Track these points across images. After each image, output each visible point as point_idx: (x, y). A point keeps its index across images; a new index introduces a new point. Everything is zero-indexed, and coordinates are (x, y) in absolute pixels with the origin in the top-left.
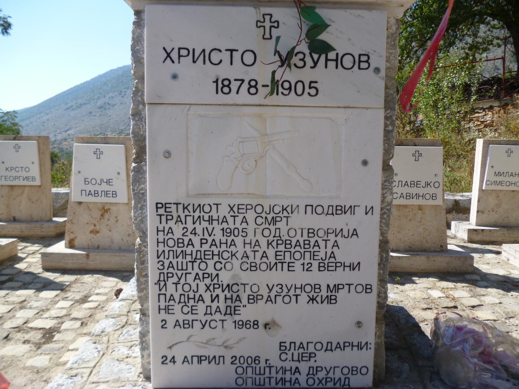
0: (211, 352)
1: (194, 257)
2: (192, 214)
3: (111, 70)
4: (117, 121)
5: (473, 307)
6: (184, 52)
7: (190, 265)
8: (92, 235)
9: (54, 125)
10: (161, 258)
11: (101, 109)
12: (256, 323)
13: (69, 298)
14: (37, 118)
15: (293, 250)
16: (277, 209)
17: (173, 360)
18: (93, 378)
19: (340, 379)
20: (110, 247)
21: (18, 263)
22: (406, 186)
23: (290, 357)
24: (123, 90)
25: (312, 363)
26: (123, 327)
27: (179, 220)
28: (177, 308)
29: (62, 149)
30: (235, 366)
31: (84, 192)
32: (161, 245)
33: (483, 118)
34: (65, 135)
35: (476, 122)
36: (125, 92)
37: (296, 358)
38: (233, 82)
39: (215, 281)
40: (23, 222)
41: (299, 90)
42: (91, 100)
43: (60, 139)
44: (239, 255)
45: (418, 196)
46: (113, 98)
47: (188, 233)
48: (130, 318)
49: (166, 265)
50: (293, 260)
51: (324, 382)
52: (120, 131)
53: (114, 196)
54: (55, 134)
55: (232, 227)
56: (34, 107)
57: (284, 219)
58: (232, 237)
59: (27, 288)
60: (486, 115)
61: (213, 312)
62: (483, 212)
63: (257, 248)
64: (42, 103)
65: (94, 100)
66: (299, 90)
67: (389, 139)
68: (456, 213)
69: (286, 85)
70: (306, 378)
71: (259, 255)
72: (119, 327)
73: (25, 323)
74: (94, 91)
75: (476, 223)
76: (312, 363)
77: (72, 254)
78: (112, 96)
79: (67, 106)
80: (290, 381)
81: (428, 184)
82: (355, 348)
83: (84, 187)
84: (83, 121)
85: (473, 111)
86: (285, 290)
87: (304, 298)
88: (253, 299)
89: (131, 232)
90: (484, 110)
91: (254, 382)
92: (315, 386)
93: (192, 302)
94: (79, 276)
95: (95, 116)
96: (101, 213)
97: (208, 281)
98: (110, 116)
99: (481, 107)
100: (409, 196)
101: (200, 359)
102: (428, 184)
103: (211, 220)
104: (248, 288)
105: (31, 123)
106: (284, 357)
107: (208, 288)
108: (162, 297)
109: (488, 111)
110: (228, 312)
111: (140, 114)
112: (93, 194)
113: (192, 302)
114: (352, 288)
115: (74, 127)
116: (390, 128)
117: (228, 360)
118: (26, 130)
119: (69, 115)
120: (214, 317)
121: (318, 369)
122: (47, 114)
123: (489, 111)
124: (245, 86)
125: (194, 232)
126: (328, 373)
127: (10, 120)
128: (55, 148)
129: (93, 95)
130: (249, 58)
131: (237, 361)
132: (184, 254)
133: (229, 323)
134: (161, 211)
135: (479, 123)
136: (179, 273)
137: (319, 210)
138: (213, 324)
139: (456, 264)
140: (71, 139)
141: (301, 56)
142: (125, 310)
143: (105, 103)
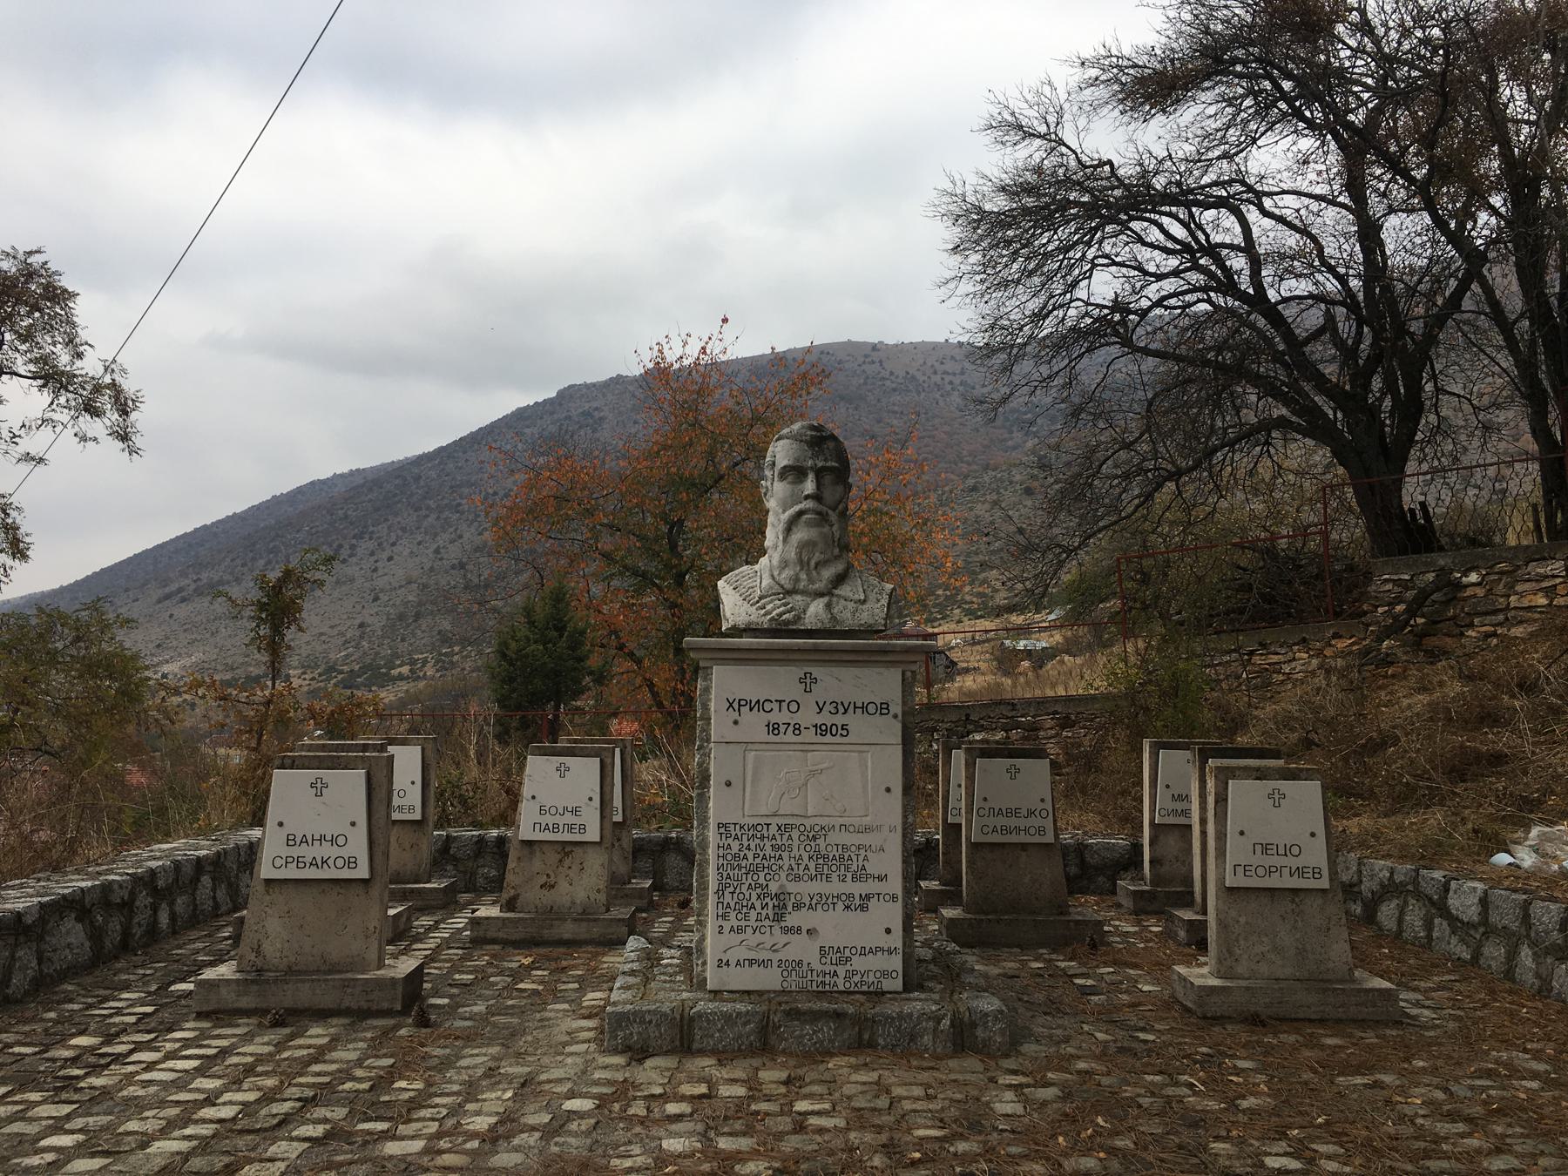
3: (312, 483)
12: (799, 929)
17: (728, 964)
25: (848, 967)
27: (736, 837)
28: (733, 915)
31: (537, 826)
44: (785, 868)
45: (1018, 830)
71: (802, 868)
74: (254, 544)
76: (848, 967)
79: (167, 590)
81: (1031, 813)
87: (840, 906)
88: (798, 906)
97: (759, 890)
102: (1031, 813)
103: (762, 838)
106: (823, 960)
117: (775, 964)
121: (855, 972)
124: (791, 728)
130: (794, 707)
133: (776, 931)
134: (722, 830)
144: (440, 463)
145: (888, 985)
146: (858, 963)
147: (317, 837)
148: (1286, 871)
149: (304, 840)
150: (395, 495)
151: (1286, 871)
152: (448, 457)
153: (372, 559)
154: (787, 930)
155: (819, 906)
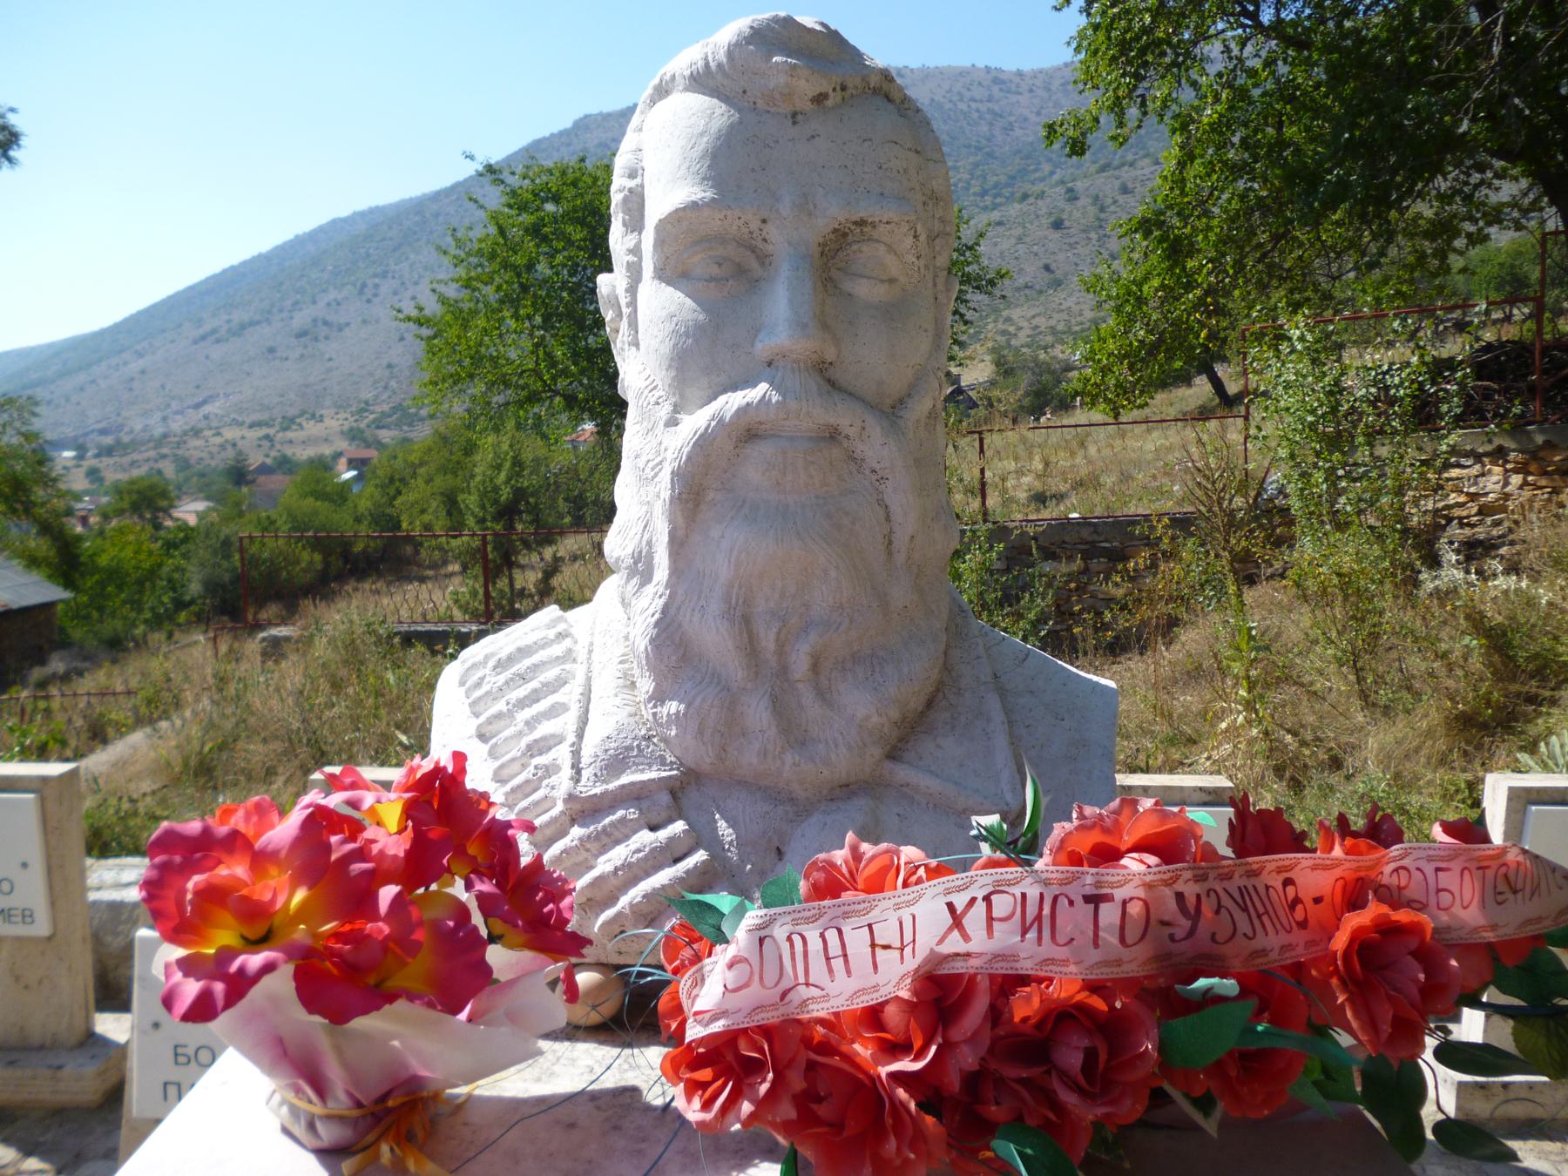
3: (334, 222)
4: (351, 374)
9: (163, 387)
11: (303, 339)
24: (370, 282)
29: (186, 460)
33: (1476, 483)
34: (194, 417)
35: (1453, 495)
36: (376, 286)
46: (338, 304)
52: (362, 405)
56: (101, 334)
60: (1483, 475)
64: (126, 321)
65: (281, 311)
74: (282, 284)
79: (201, 331)
84: (248, 374)
90: (1478, 458)
95: (286, 359)
98: (330, 359)
105: (93, 382)
109: (1492, 463)
118: (78, 404)
122: (140, 355)
123: (1494, 463)
128: (164, 456)
129: (278, 295)
135: (1462, 499)
140: (213, 432)
143: (315, 320)
150: (415, 233)
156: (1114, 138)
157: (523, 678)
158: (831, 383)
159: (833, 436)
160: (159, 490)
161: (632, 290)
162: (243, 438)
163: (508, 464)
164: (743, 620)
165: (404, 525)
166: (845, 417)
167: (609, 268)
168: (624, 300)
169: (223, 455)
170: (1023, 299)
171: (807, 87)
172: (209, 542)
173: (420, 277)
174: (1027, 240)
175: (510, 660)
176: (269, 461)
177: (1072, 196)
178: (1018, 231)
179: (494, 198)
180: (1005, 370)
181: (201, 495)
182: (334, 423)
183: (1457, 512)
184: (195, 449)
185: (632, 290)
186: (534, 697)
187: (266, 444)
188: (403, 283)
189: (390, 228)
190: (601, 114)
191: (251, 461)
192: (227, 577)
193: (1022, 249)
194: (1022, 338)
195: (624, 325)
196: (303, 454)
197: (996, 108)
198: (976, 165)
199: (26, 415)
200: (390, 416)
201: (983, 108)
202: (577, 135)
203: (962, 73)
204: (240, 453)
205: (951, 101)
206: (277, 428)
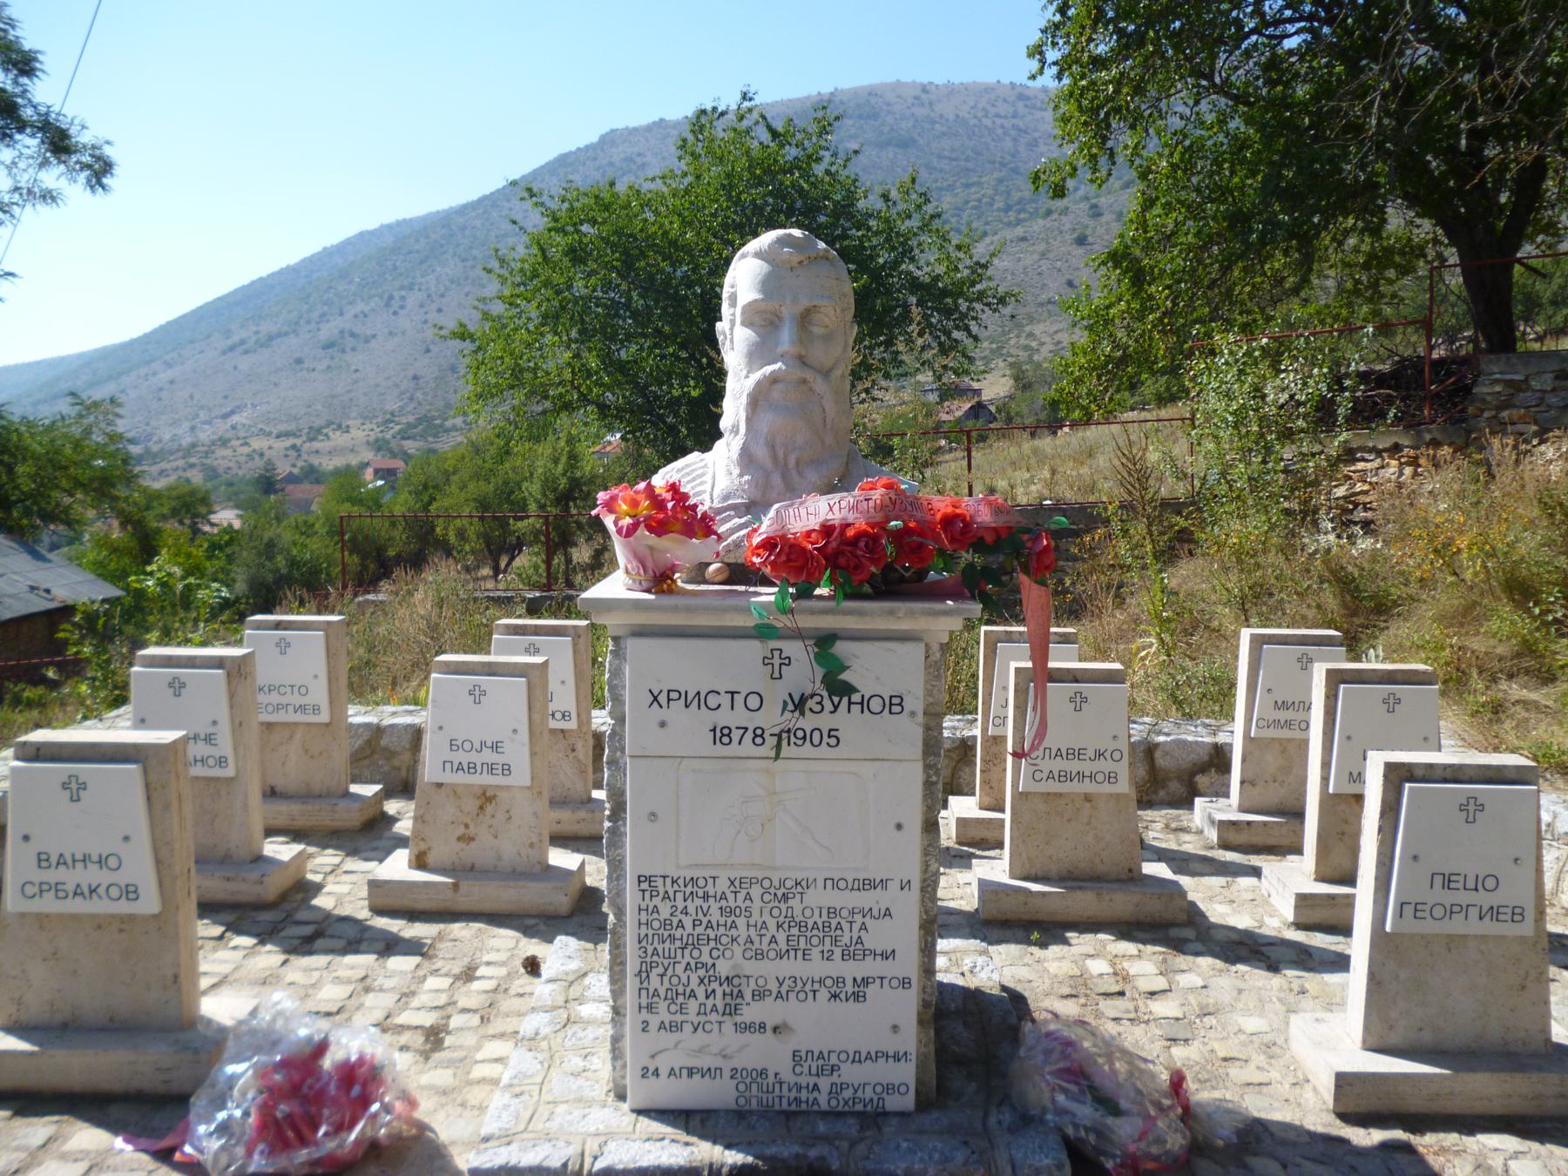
0: (705, 1062)
1: (685, 941)
2: (682, 888)
3: (362, 234)
4: (377, 385)
5: (1153, 994)
6: (674, 695)
7: (679, 951)
8: (462, 845)
9: (191, 397)
10: (644, 944)
12: (762, 1026)
13: (442, 972)
14: (139, 377)
15: (809, 934)
16: (789, 884)
17: (656, 1073)
18: (546, 1097)
19: (872, 1100)
20: (495, 867)
21: (315, 896)
22: (1059, 758)
23: (806, 1070)
24: (396, 294)
25: (835, 1078)
26: (565, 1026)
27: (666, 897)
28: (663, 1006)
29: (214, 469)
30: (735, 1082)
31: (448, 766)
32: (643, 927)
33: (1377, 475)
34: (222, 427)
36: (403, 298)
37: (814, 1071)
38: (734, 730)
39: (711, 972)
40: (292, 797)
41: (816, 740)
42: (302, 322)
43: (207, 441)
44: (741, 940)
45: (1081, 776)
46: (366, 316)
47: (678, 913)
48: (571, 1011)
49: (650, 952)
50: (809, 946)
51: (851, 1103)
52: (388, 416)
53: (506, 772)
54: (193, 423)
55: (733, 905)
57: (798, 896)
58: (733, 917)
59: (357, 952)
60: (1383, 467)
61: (708, 1012)
62: (1253, 784)
63: (763, 931)
64: (155, 332)
65: (309, 322)
66: (816, 740)
67: (932, 793)
68: (1216, 772)
69: (800, 734)
70: (827, 1097)
71: (766, 940)
72: (558, 1027)
73: (388, 1017)
74: (309, 296)
75: (1240, 805)
76: (835, 1078)
77: (426, 884)
78: (362, 312)
79: (229, 342)
80: (807, 1102)
81: (1100, 754)
82: (891, 1060)
83: (449, 756)
84: (276, 385)
85: (1349, 455)
86: (800, 984)
87: (823, 994)
88: (759, 995)
89: (535, 840)
90: (1379, 453)
91: (760, 1102)
92: (840, 1108)
93: (681, 999)
94: (442, 926)
95: (314, 370)
96: (478, 803)
97: (702, 972)
98: (356, 371)
99: (1371, 445)
100: (1065, 776)
101: (691, 1072)
102: (1100, 754)
103: (706, 897)
104: (752, 981)
106: (798, 1069)
107: (702, 981)
108: (644, 993)
109: (1390, 458)
110: (727, 1011)
111: (618, 763)
112: (466, 768)
113: (681, 999)
114: (886, 982)
115: (249, 403)
116: (934, 779)
117: (727, 1074)
119: (235, 368)
120: (709, 1018)
121: (843, 1086)
122: (169, 365)
123: (1391, 458)
124: (749, 735)
125: (685, 912)
126: (856, 1091)
127: (103, 425)
128: (192, 466)
129: (306, 307)
130: (754, 702)
131: (738, 1075)
132: (672, 938)
133: (728, 1026)
134: (645, 886)
135: (1366, 487)
136: (666, 962)
137: (842, 884)
138: (708, 1027)
139: (1154, 907)
141: (818, 699)
142: (560, 1000)
143: (342, 332)
144: (484, 212)
145: (893, 1103)
146: (851, 1074)
147: (79, 856)
148: (1474, 912)
149: (61, 861)
150: (442, 246)
151: (1474, 912)
152: (492, 206)
153: (423, 310)
154: (747, 1028)
155: (792, 996)
156: (1092, 181)
157: (688, 474)
158: (804, 363)
159: (804, 381)
160: (199, 496)
161: (732, 329)
162: (270, 448)
163: (564, 460)
164: (772, 447)
165: (438, 530)
166: (809, 375)
167: (721, 320)
168: (728, 333)
169: (251, 465)
170: (1046, 314)
171: (796, 259)
172: (252, 544)
173: (447, 289)
174: (1051, 256)
175: (683, 468)
176: (296, 471)
177: (1096, 212)
178: (1042, 247)
179: (536, 221)
180: (1023, 383)
181: (231, 504)
182: (360, 433)
183: (1361, 499)
184: (223, 458)
185: (732, 329)
186: (694, 479)
187: (293, 453)
188: (429, 296)
189: (417, 240)
190: (627, 129)
191: (279, 471)
192: (270, 578)
193: (1045, 265)
194: (1045, 351)
195: (728, 342)
196: (329, 464)
197: (1021, 124)
198: (1000, 181)
199: (110, 417)
200: (415, 427)
201: (1008, 123)
202: (603, 150)
203: (987, 89)
204: (269, 462)
205: (975, 117)
206: (304, 438)
